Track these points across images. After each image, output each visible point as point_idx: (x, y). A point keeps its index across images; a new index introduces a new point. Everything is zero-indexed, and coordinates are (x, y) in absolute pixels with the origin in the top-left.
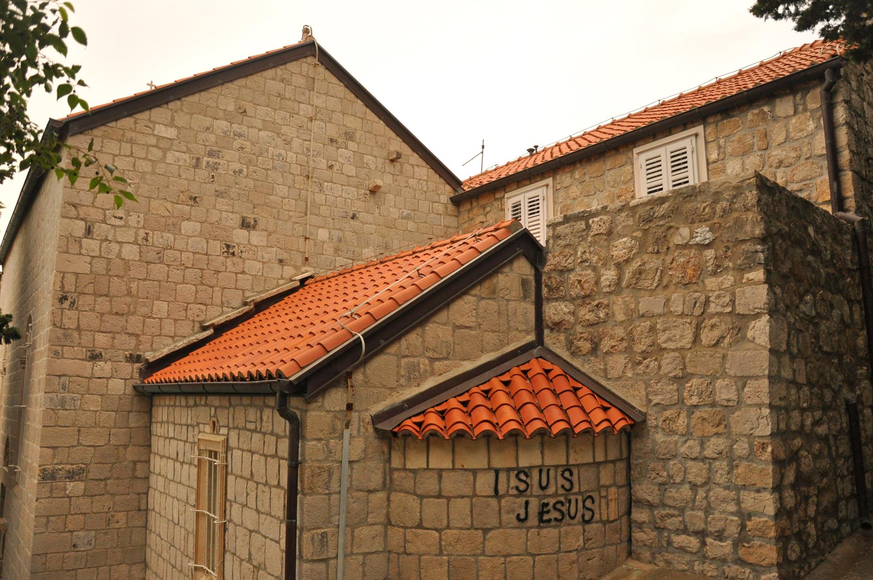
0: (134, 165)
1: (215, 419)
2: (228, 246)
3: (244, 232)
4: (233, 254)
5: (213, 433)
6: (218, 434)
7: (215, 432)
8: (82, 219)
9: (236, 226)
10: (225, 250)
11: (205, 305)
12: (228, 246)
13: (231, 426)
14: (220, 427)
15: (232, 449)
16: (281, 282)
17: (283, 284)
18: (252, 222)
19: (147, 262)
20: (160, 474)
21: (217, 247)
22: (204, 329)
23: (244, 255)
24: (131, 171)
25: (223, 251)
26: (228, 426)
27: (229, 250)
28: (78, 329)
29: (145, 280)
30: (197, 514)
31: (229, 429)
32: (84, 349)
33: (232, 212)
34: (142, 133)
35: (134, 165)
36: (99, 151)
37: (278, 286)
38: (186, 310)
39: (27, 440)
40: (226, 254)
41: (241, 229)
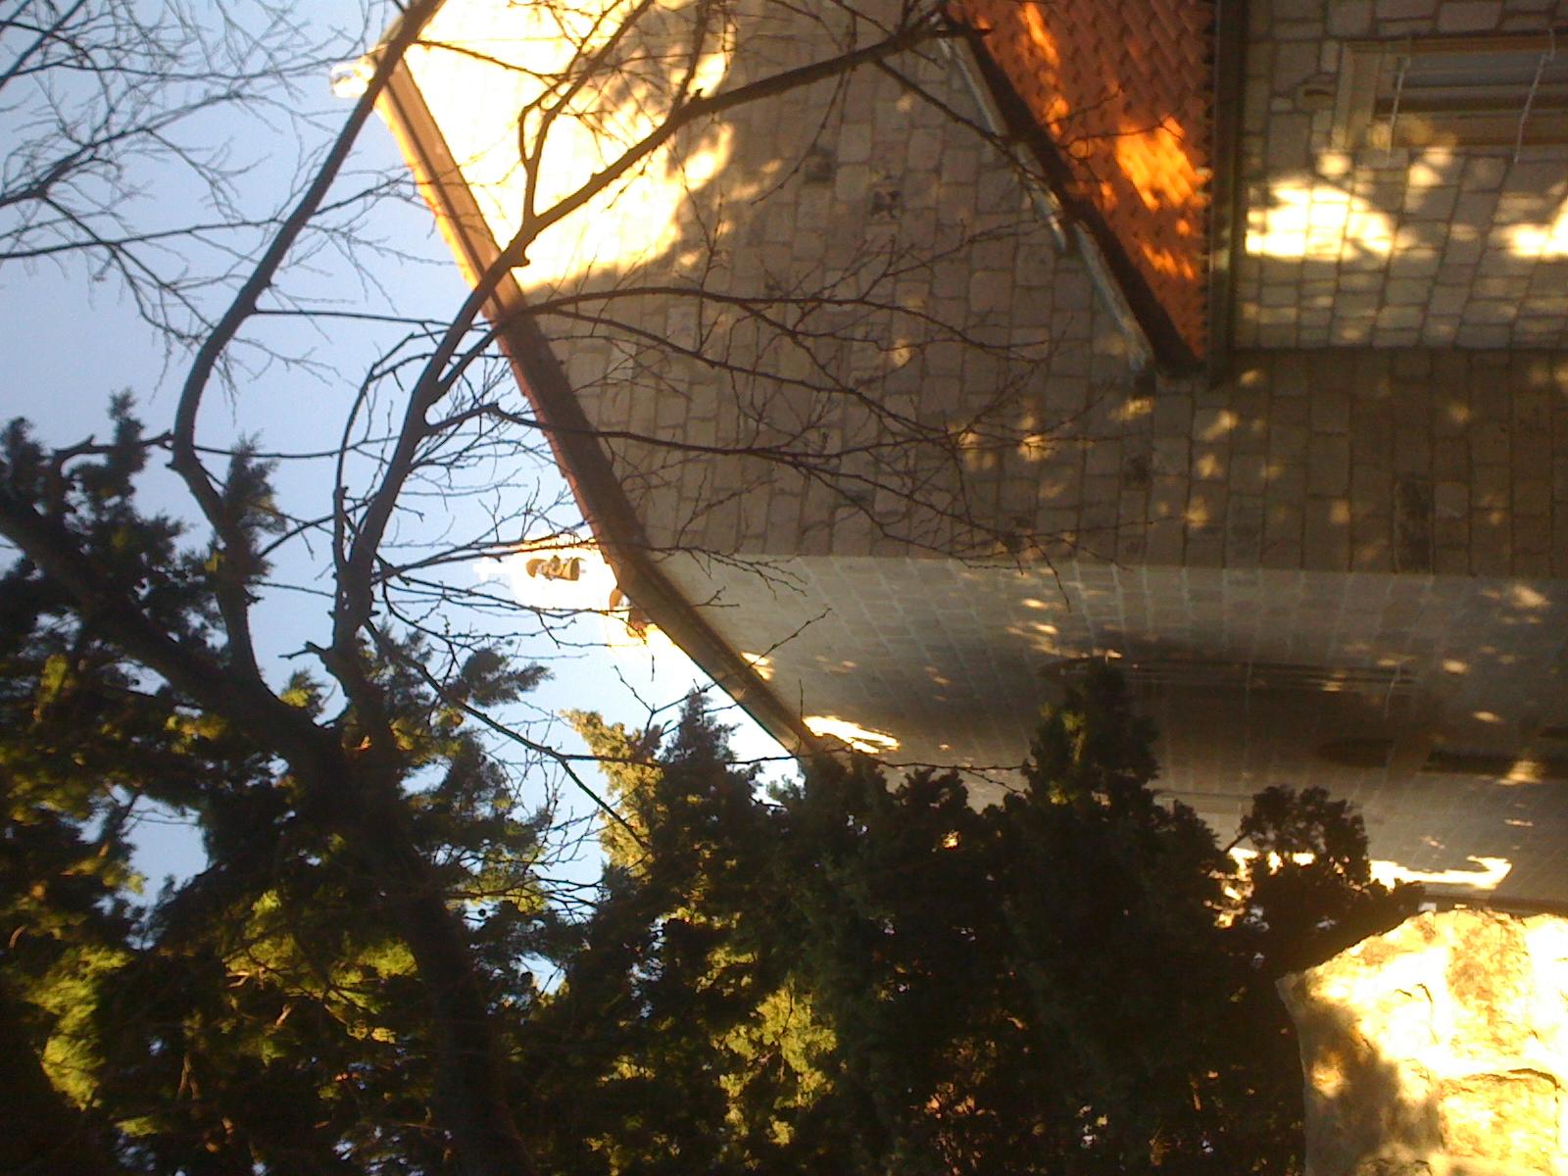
0: (703, 419)
1: (1301, 90)
2: (878, 207)
3: (842, 176)
4: (894, 195)
5: (1333, 95)
6: (1335, 78)
7: (1330, 89)
8: (832, 514)
9: (828, 194)
10: (885, 213)
11: (1016, 248)
12: (878, 207)
13: (1315, 29)
14: (1319, 72)
15: (1375, 22)
16: (957, 83)
17: (963, 77)
18: (815, 160)
19: (922, 379)
20: (1425, 306)
21: (880, 232)
22: (1073, 248)
23: (897, 172)
24: (718, 423)
25: (888, 219)
26: (1319, 41)
27: (886, 203)
28: (1078, 508)
29: (962, 379)
30: (1526, 141)
31: (1327, 35)
32: (1125, 494)
33: (797, 204)
34: (631, 408)
35: (703, 419)
36: (679, 492)
37: (967, 89)
38: (1029, 289)
39: (1323, 672)
40: (896, 212)
41: (834, 182)
